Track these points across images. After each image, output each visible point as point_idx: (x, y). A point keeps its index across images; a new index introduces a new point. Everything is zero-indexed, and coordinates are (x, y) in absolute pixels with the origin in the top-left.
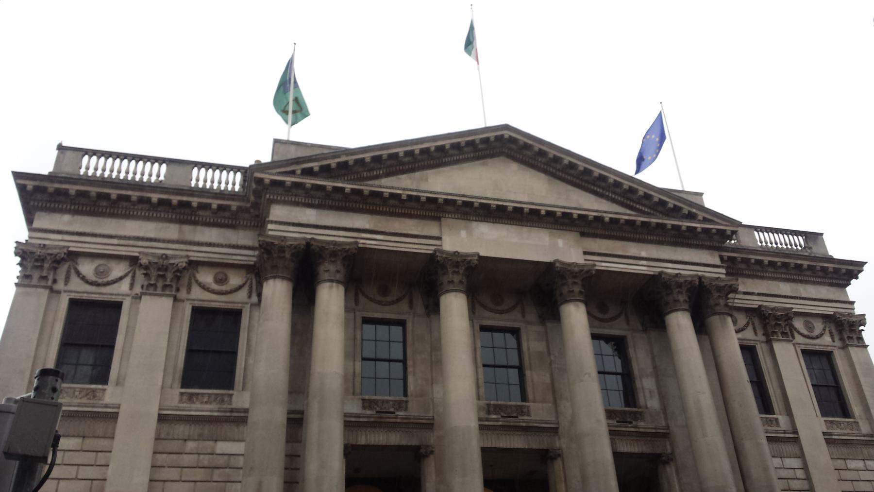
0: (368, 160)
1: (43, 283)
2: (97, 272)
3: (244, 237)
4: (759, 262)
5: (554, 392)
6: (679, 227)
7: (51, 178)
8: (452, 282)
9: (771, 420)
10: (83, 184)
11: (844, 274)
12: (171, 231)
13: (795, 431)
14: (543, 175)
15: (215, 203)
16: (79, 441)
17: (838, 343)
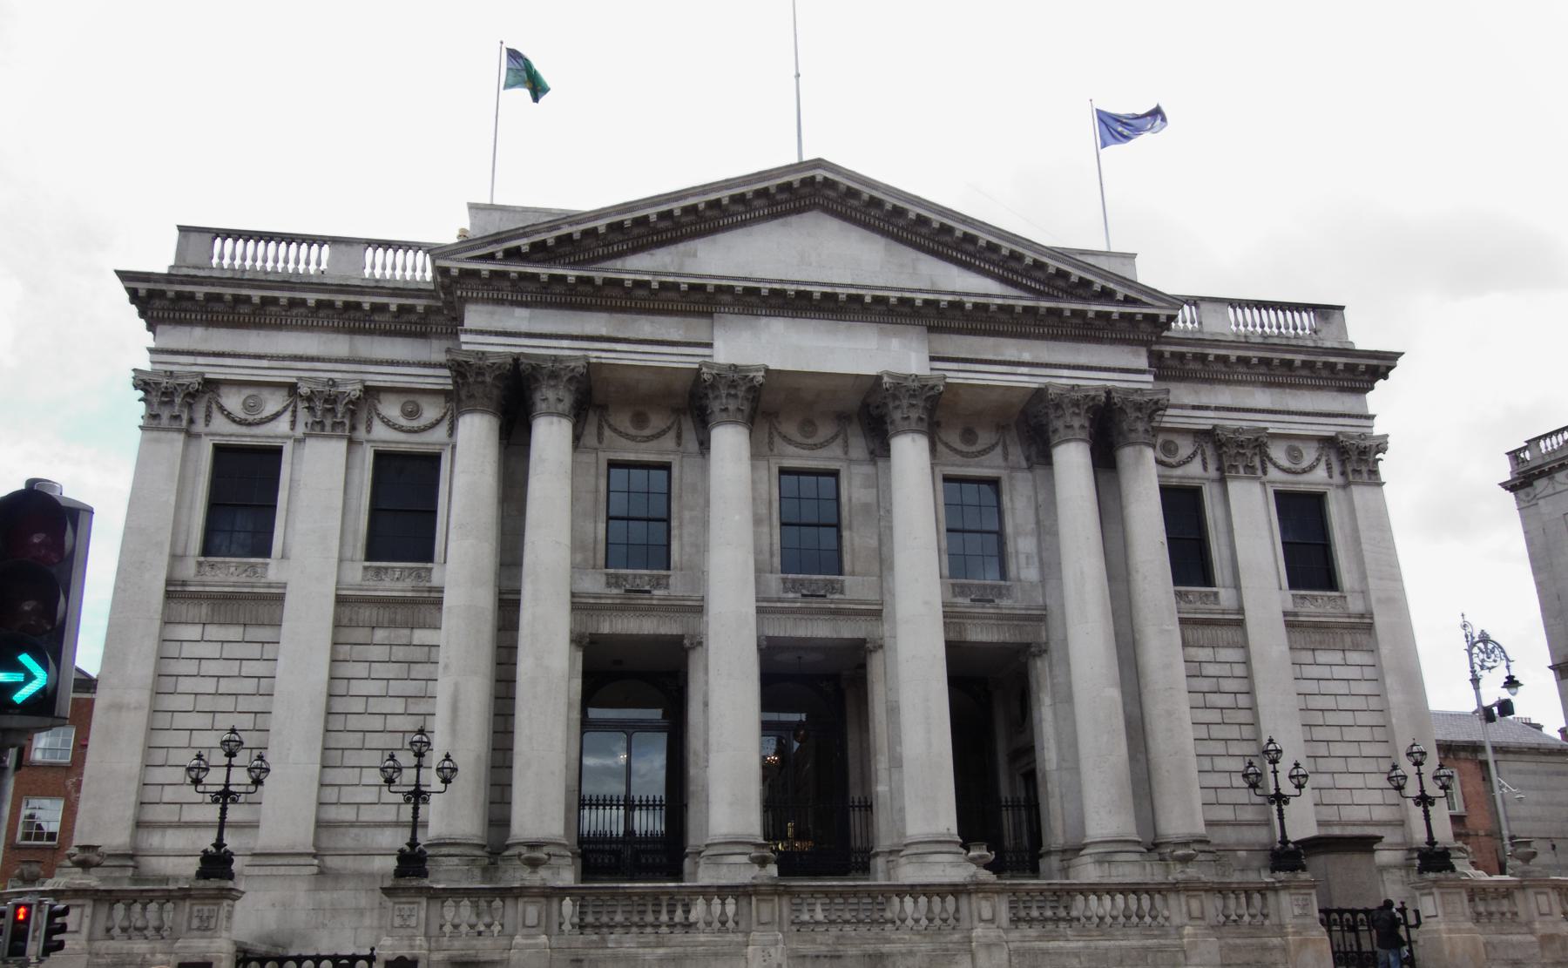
0: (602, 230)
1: (175, 425)
2: (246, 407)
3: (435, 351)
4: (1223, 360)
5: (881, 562)
6: (1083, 313)
7: (169, 278)
8: (726, 410)
9: (1207, 595)
10: (213, 285)
11: (1363, 373)
12: (339, 345)
13: (1241, 610)
14: (877, 237)
15: (393, 303)
16: (199, 628)
17: (1338, 479)
